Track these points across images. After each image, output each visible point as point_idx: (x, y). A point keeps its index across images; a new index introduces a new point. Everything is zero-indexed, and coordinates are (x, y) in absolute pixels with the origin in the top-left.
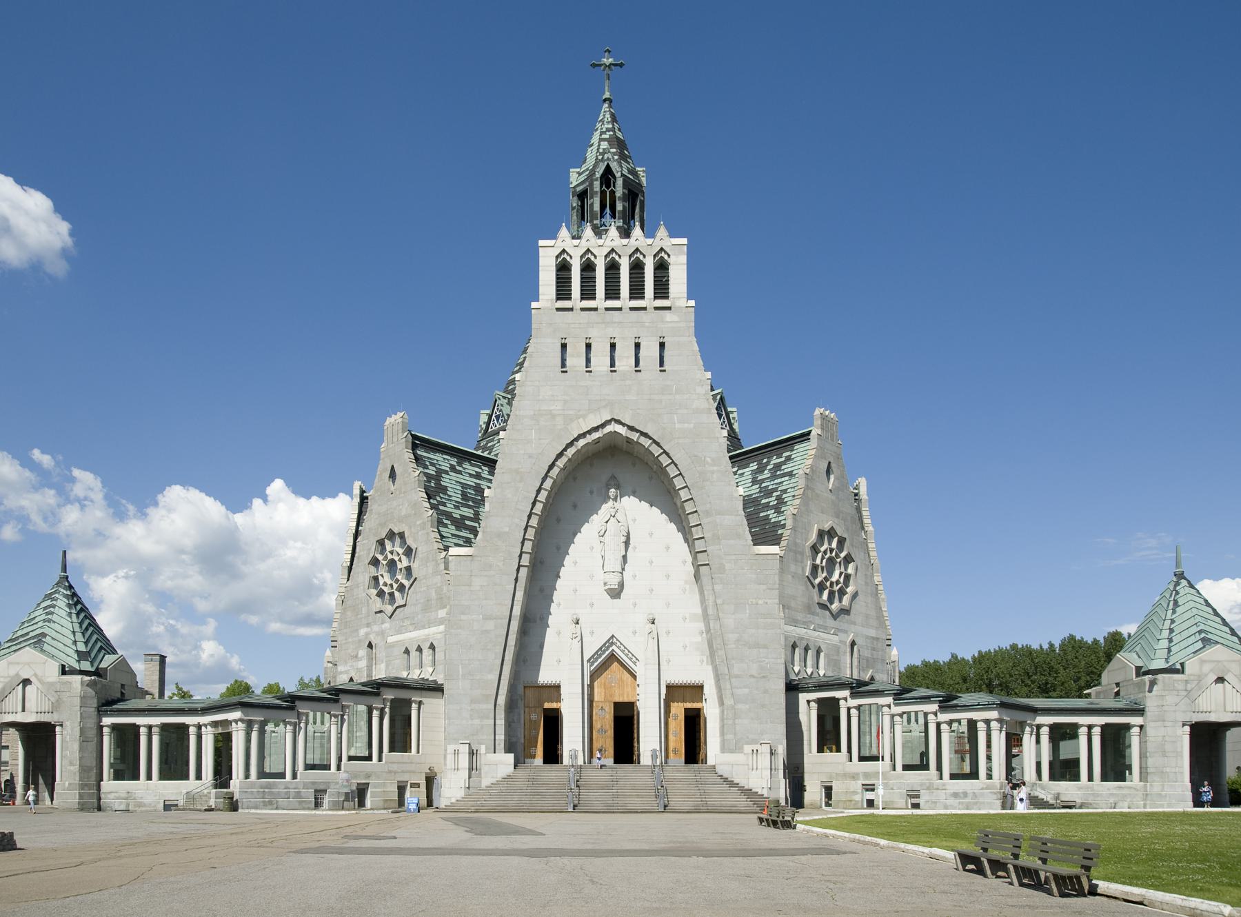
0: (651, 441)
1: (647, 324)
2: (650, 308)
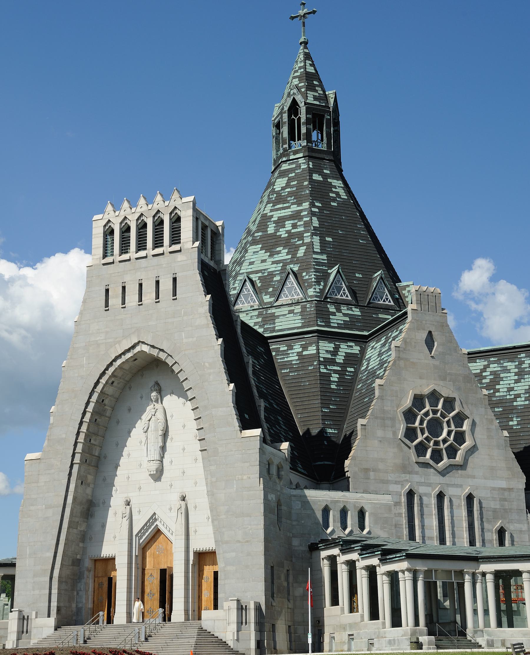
0: (167, 354)
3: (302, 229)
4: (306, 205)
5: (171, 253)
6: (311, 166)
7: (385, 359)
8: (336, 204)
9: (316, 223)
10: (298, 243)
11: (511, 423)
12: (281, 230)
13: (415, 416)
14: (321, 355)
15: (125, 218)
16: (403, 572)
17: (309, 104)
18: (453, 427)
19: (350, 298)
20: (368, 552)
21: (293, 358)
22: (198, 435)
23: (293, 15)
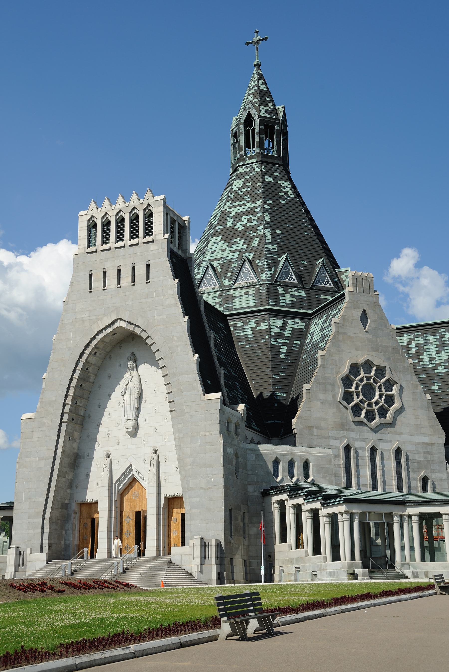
1: (139, 254)
2: (141, 244)
3: (256, 223)
4: (259, 203)
6: (263, 170)
8: (284, 202)
9: (267, 218)
11: (433, 388)
12: (238, 224)
13: (352, 382)
14: (272, 330)
16: (341, 514)
18: (384, 391)
21: (248, 332)
22: (167, 398)
23: (248, 42)
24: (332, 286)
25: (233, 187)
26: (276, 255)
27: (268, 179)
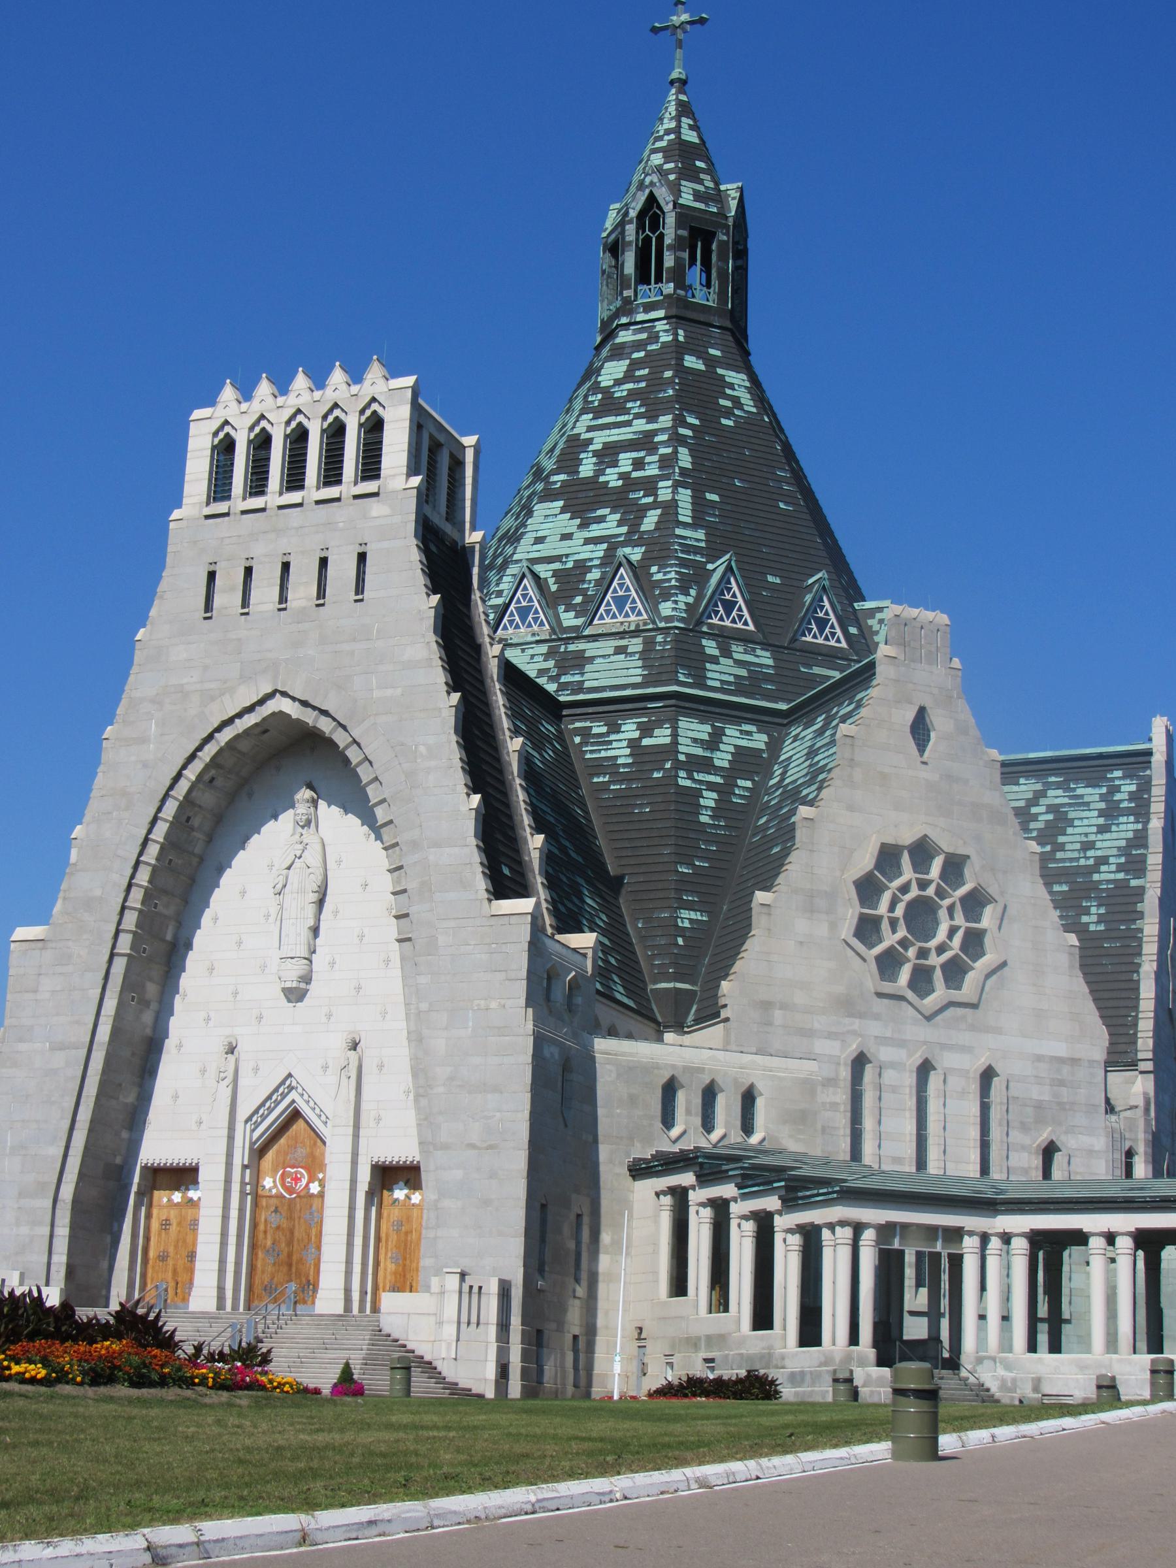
1: (341, 525)
2: (348, 498)
3: (656, 472)
4: (666, 421)
5: (356, 497)
6: (681, 339)
7: (821, 764)
8: (731, 423)
9: (685, 459)
10: (645, 501)
11: (1085, 919)
12: (608, 471)
13: (881, 889)
14: (681, 749)
15: (263, 417)
16: (831, 1227)
17: (682, 206)
18: (960, 920)
19: (751, 627)
20: (759, 1181)
21: (619, 751)
22: (394, 906)
23: (657, 25)
24: (844, 645)
25: (600, 379)
26: (702, 555)
27: (691, 362)
